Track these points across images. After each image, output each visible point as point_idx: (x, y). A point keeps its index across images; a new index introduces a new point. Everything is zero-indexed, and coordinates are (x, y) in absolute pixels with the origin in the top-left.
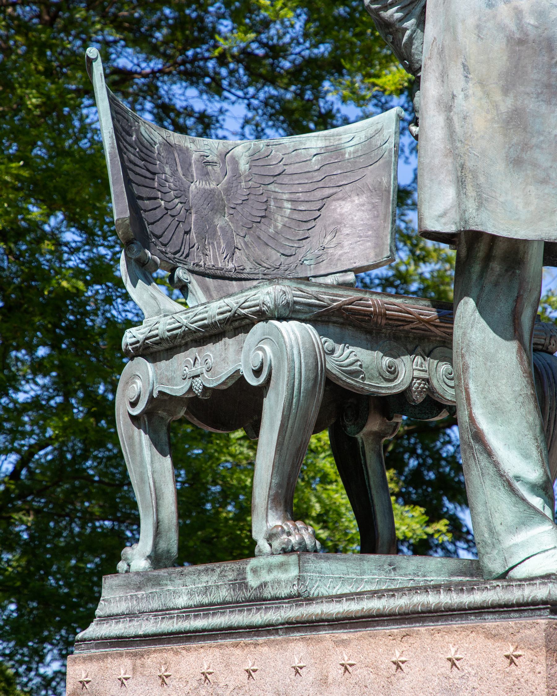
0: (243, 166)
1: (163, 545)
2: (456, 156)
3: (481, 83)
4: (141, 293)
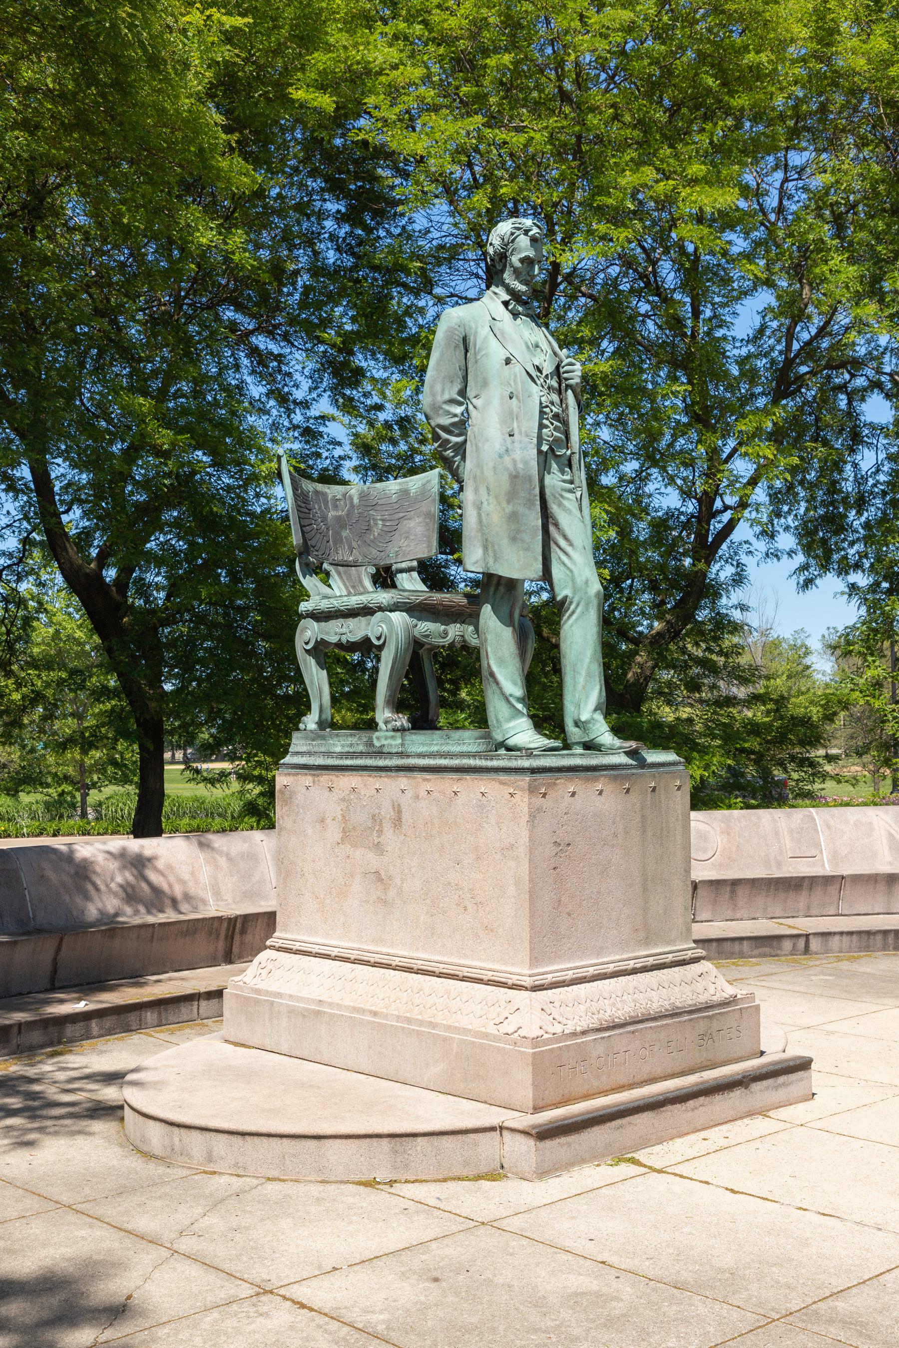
0: (356, 501)
1: (324, 717)
2: (483, 534)
3: (496, 497)
4: (310, 582)
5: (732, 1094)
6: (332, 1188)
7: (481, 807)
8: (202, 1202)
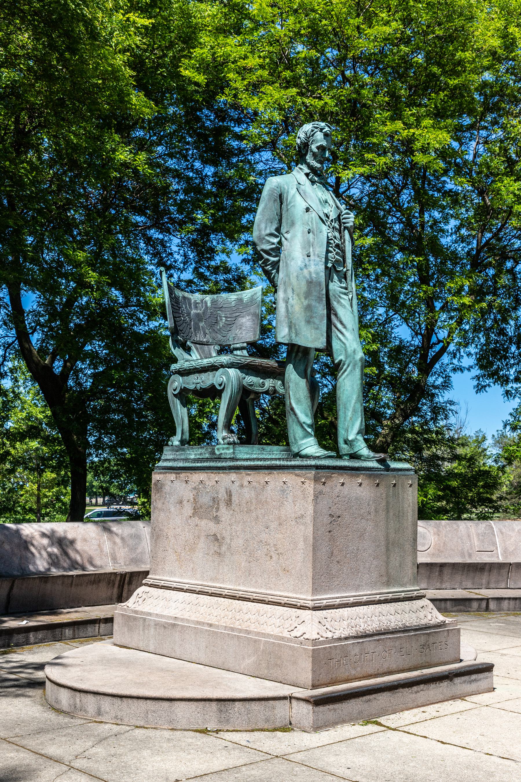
0: (209, 304)
2: (289, 319)
3: (298, 295)
4: (177, 352)
5: (441, 684)
6: (178, 733)
7: (283, 491)
8: (92, 739)
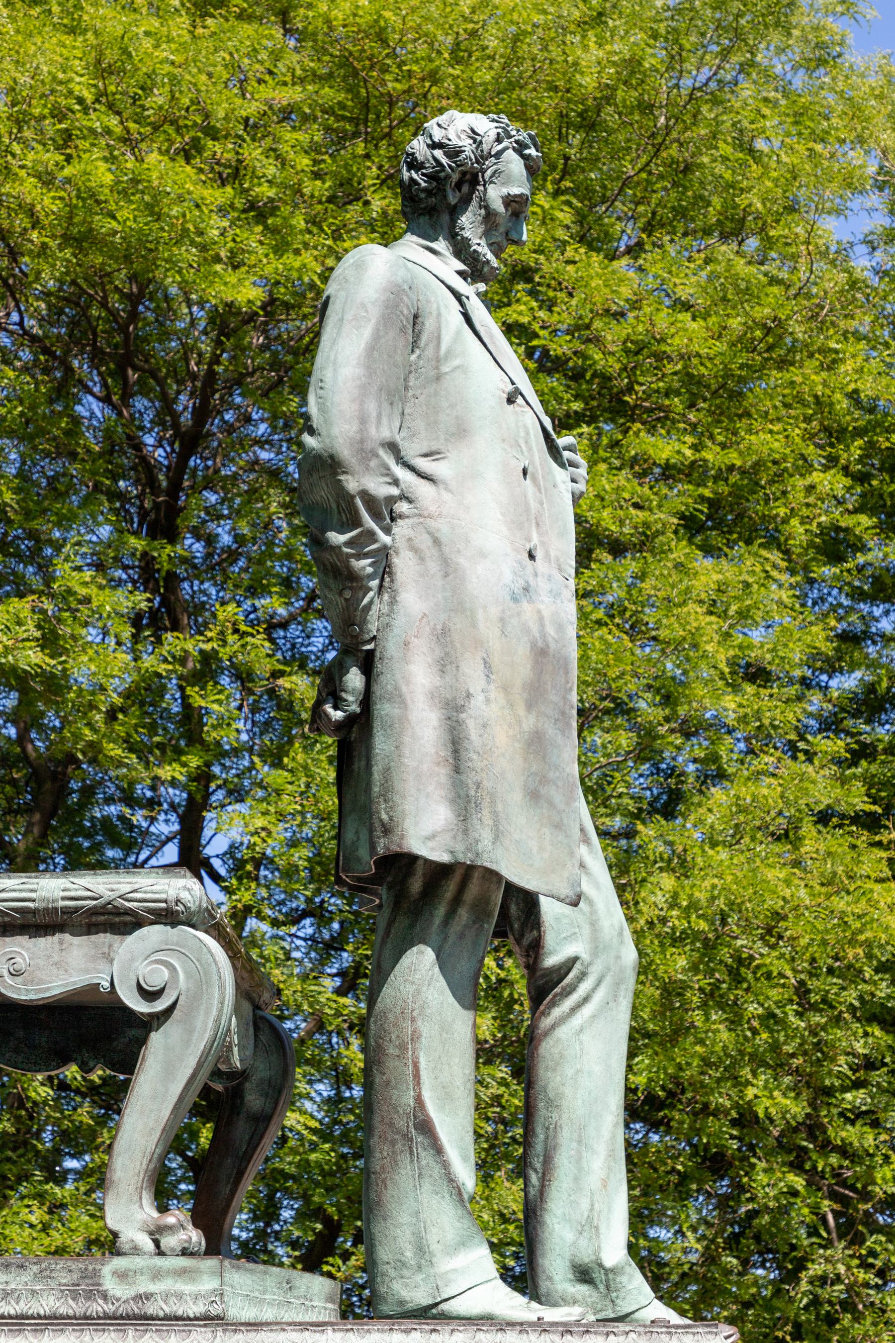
3: (505, 689)
